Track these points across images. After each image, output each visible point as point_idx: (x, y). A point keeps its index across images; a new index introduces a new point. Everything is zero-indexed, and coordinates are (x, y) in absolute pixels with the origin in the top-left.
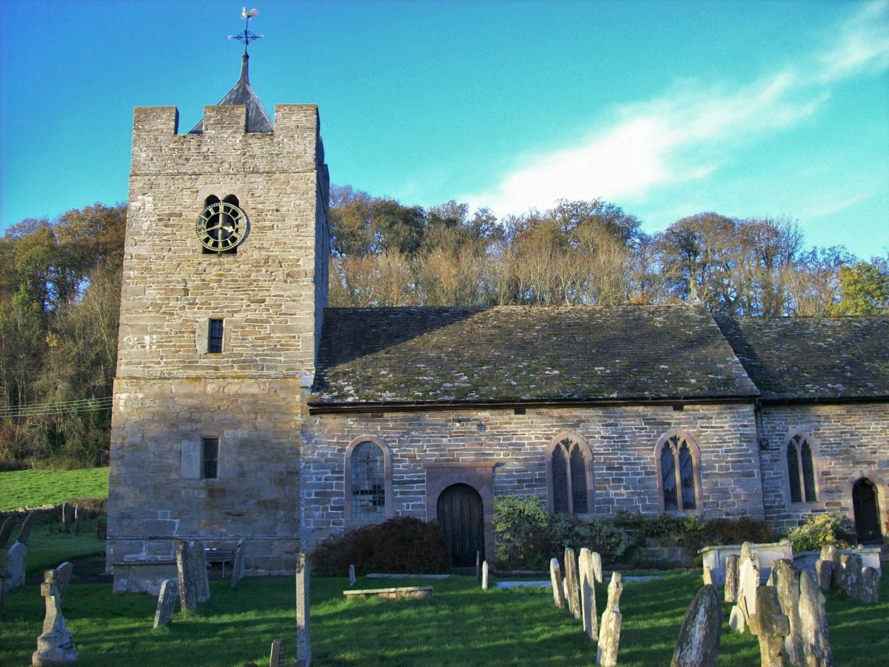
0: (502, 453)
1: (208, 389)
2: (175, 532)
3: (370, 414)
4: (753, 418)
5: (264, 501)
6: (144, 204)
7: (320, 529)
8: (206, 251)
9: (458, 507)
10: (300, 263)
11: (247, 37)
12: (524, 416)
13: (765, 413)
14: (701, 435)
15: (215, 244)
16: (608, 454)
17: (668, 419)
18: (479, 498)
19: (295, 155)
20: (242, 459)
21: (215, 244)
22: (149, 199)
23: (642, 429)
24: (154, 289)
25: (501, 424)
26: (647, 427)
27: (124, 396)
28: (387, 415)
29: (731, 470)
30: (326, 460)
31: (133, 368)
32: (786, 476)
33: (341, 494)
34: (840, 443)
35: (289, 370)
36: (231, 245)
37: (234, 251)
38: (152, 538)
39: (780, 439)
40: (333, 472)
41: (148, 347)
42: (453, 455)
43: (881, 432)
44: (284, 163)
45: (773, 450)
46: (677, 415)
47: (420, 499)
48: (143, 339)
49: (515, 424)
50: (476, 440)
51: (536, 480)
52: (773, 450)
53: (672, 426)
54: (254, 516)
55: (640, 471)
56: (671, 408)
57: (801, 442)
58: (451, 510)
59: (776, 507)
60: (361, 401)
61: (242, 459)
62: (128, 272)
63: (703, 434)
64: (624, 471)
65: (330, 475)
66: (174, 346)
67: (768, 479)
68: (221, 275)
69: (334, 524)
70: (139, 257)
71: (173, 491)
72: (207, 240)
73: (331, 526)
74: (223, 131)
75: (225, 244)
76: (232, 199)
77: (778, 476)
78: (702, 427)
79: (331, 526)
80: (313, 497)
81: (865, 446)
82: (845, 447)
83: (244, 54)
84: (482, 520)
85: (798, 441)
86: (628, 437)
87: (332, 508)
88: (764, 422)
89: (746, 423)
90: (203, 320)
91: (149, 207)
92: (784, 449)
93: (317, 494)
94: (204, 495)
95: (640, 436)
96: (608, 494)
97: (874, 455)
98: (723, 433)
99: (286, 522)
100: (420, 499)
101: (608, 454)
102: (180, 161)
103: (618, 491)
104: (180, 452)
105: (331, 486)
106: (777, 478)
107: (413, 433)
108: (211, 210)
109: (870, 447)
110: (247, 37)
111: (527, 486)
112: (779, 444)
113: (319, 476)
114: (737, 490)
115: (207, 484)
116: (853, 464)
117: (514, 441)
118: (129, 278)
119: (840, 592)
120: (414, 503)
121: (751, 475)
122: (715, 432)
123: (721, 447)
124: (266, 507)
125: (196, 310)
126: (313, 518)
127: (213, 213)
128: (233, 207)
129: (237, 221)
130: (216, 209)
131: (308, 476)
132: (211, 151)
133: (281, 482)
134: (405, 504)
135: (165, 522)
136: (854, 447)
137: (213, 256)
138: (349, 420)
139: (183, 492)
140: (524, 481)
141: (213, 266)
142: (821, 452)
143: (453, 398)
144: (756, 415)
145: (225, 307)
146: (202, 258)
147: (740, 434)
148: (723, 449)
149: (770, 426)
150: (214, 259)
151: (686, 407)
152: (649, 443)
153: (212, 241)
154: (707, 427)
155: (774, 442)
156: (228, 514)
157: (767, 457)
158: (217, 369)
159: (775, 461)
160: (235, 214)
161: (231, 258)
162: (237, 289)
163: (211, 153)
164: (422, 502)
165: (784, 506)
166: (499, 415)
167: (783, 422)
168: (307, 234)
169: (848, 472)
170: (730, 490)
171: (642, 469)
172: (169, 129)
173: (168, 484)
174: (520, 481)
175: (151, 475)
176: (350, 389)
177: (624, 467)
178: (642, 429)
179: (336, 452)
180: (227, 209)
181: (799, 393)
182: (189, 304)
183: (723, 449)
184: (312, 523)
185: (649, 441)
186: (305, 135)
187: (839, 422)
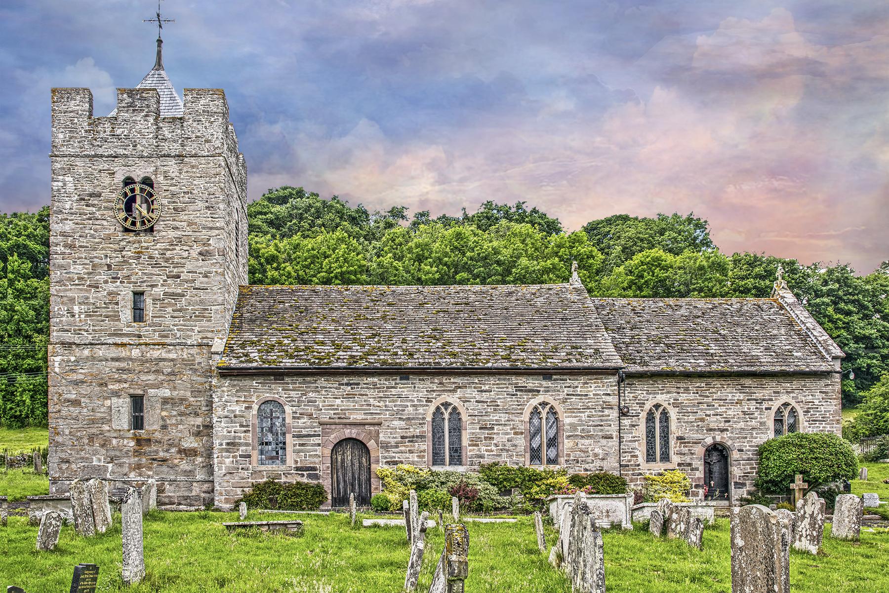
0: (388, 413)
1: (133, 354)
2: (108, 474)
3: (272, 378)
4: (616, 388)
5: (185, 450)
6: (65, 184)
7: (231, 473)
8: (126, 230)
9: (349, 458)
10: (211, 242)
13: (628, 384)
15: (134, 224)
16: (482, 416)
17: (538, 387)
18: (368, 451)
19: (203, 139)
20: (164, 413)
21: (134, 224)
22: (69, 179)
23: (513, 395)
24: (80, 265)
25: (388, 388)
27: (58, 359)
28: (287, 379)
30: (235, 416)
31: (64, 334)
32: (643, 439)
33: (247, 445)
35: (203, 338)
36: (148, 225)
37: (151, 230)
40: (242, 426)
41: (77, 316)
42: (345, 414)
43: (737, 403)
44: (190, 148)
45: (633, 416)
47: (316, 451)
48: (73, 308)
49: (400, 388)
50: (365, 401)
51: (417, 437)
52: (633, 416)
53: (541, 393)
54: (176, 461)
55: (509, 431)
56: (542, 377)
57: (661, 409)
58: (343, 461)
59: (631, 465)
60: (263, 366)
61: (164, 413)
62: (55, 248)
64: (495, 431)
65: (238, 428)
66: (101, 315)
67: (626, 441)
68: (139, 253)
69: (242, 469)
70: (63, 234)
71: (106, 440)
72: (126, 219)
73: (240, 471)
74: (135, 114)
75: (143, 223)
76: (147, 182)
79: (240, 471)
80: (224, 446)
84: (370, 469)
85: (657, 410)
86: (501, 402)
87: (241, 456)
88: (626, 392)
90: (126, 294)
91: (70, 187)
92: (643, 415)
93: (228, 444)
94: (132, 444)
96: (479, 450)
97: (727, 424)
99: (203, 467)
100: (316, 451)
101: (482, 416)
102: (96, 143)
103: (489, 448)
104: (110, 407)
105: (240, 438)
107: (310, 394)
108: (127, 191)
109: (725, 416)
111: (409, 441)
113: (229, 429)
114: (596, 450)
115: (135, 434)
116: (707, 431)
117: (399, 403)
118: (56, 253)
120: (311, 453)
122: (580, 399)
123: (584, 412)
124: (186, 454)
125: (118, 283)
126: (225, 464)
127: (130, 195)
128: (148, 189)
129: (152, 202)
130: (133, 190)
131: (220, 429)
132: (125, 133)
133: (198, 434)
134: (303, 454)
135: (99, 466)
136: (709, 416)
137: (132, 234)
138: (254, 382)
139: (114, 441)
140: (406, 437)
141: (131, 244)
142: (678, 419)
143: (345, 365)
144: (619, 385)
145: (144, 282)
147: (603, 402)
148: (586, 414)
149: (632, 395)
150: (131, 237)
151: (554, 377)
152: (519, 407)
153: (130, 219)
154: (573, 395)
156: (154, 459)
157: (626, 422)
158: (140, 336)
159: (634, 426)
160: (151, 195)
161: (149, 238)
162: (156, 265)
163: (125, 135)
164: (318, 453)
165: (639, 465)
167: (645, 392)
168: (217, 216)
169: (701, 438)
171: (511, 429)
172: (84, 111)
173: (100, 434)
174: (402, 437)
175: (86, 426)
176: (255, 355)
177: (496, 427)
178: (513, 395)
179: (243, 409)
180: (142, 190)
181: (661, 367)
182: (113, 278)
184: (224, 468)
185: (518, 405)
186: (212, 119)
187: (697, 393)
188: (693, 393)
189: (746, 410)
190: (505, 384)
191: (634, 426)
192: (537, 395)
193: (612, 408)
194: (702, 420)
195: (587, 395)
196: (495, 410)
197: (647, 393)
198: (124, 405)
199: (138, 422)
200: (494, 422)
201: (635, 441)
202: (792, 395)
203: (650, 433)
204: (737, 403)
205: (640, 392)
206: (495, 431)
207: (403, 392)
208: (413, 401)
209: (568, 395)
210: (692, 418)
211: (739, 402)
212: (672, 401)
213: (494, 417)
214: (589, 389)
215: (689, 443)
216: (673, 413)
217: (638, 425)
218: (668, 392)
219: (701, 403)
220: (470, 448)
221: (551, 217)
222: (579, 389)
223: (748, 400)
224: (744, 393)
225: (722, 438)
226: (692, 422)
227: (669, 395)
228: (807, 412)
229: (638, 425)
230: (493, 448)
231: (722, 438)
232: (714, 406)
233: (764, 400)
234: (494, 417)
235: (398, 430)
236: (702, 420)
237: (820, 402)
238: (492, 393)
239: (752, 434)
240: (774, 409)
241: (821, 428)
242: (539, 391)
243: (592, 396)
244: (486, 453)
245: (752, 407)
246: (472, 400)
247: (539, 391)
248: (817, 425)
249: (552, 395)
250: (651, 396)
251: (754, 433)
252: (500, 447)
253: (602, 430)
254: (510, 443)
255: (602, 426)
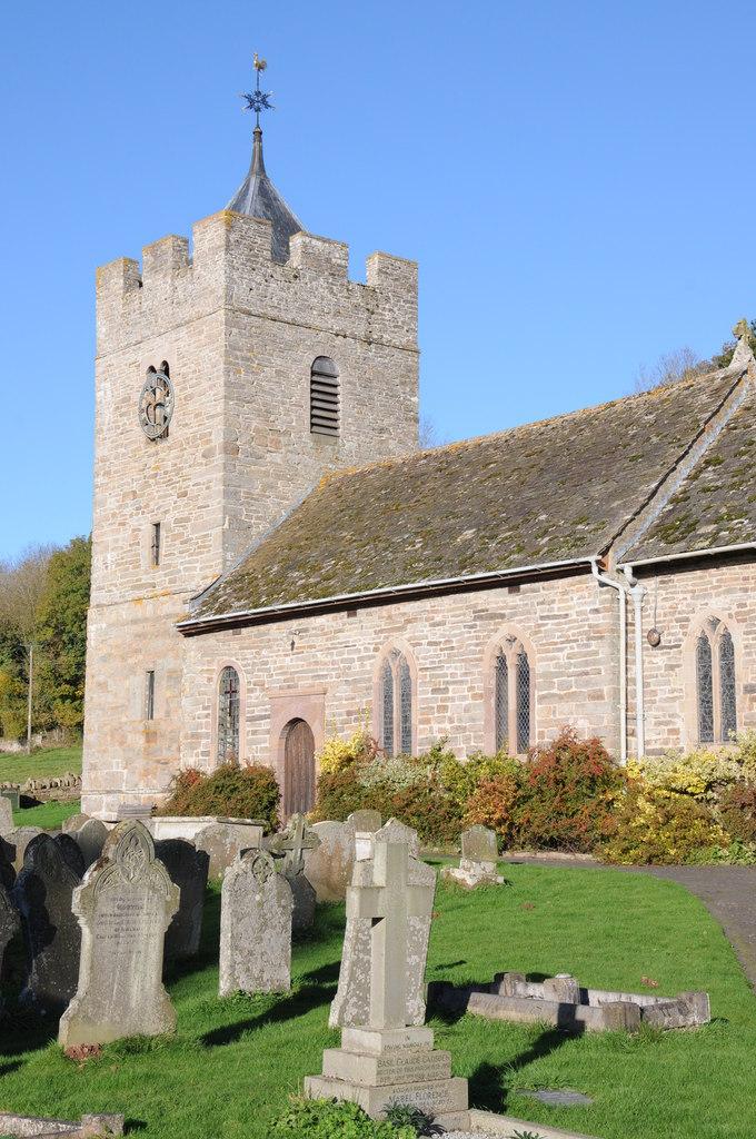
11: (258, 102)
14: (540, 632)
26: (478, 623)
29: (574, 689)
45: (671, 648)
52: (671, 648)
63: (543, 629)
64: (450, 694)
77: (676, 694)
78: (542, 618)
83: (253, 129)
88: (659, 599)
95: (469, 638)
98: (566, 627)
110: (258, 102)
112: (680, 636)
117: (345, 656)
119: (451, 888)
121: (600, 697)
122: (558, 624)
142: (746, 647)
146: (152, 448)
148: (566, 652)
152: (478, 649)
154: (548, 617)
155: (673, 634)
159: (672, 667)
167: (689, 596)
178: (471, 627)
183: (566, 652)
190: (461, 608)
191: (672, 667)
192: (500, 624)
193: (601, 638)
197: (692, 598)
200: (449, 679)
203: (705, 678)
205: (681, 596)
206: (450, 694)
207: (350, 636)
208: (360, 651)
209: (542, 618)
212: (735, 609)
213: (449, 669)
214: (571, 603)
217: (678, 666)
218: (729, 591)
220: (422, 726)
222: (555, 606)
227: (730, 597)
229: (678, 666)
234: (449, 669)
235: (344, 702)
238: (446, 627)
243: (574, 617)
246: (423, 641)
249: (521, 621)
250: (699, 602)
252: (456, 724)
254: (467, 715)
255: (587, 674)
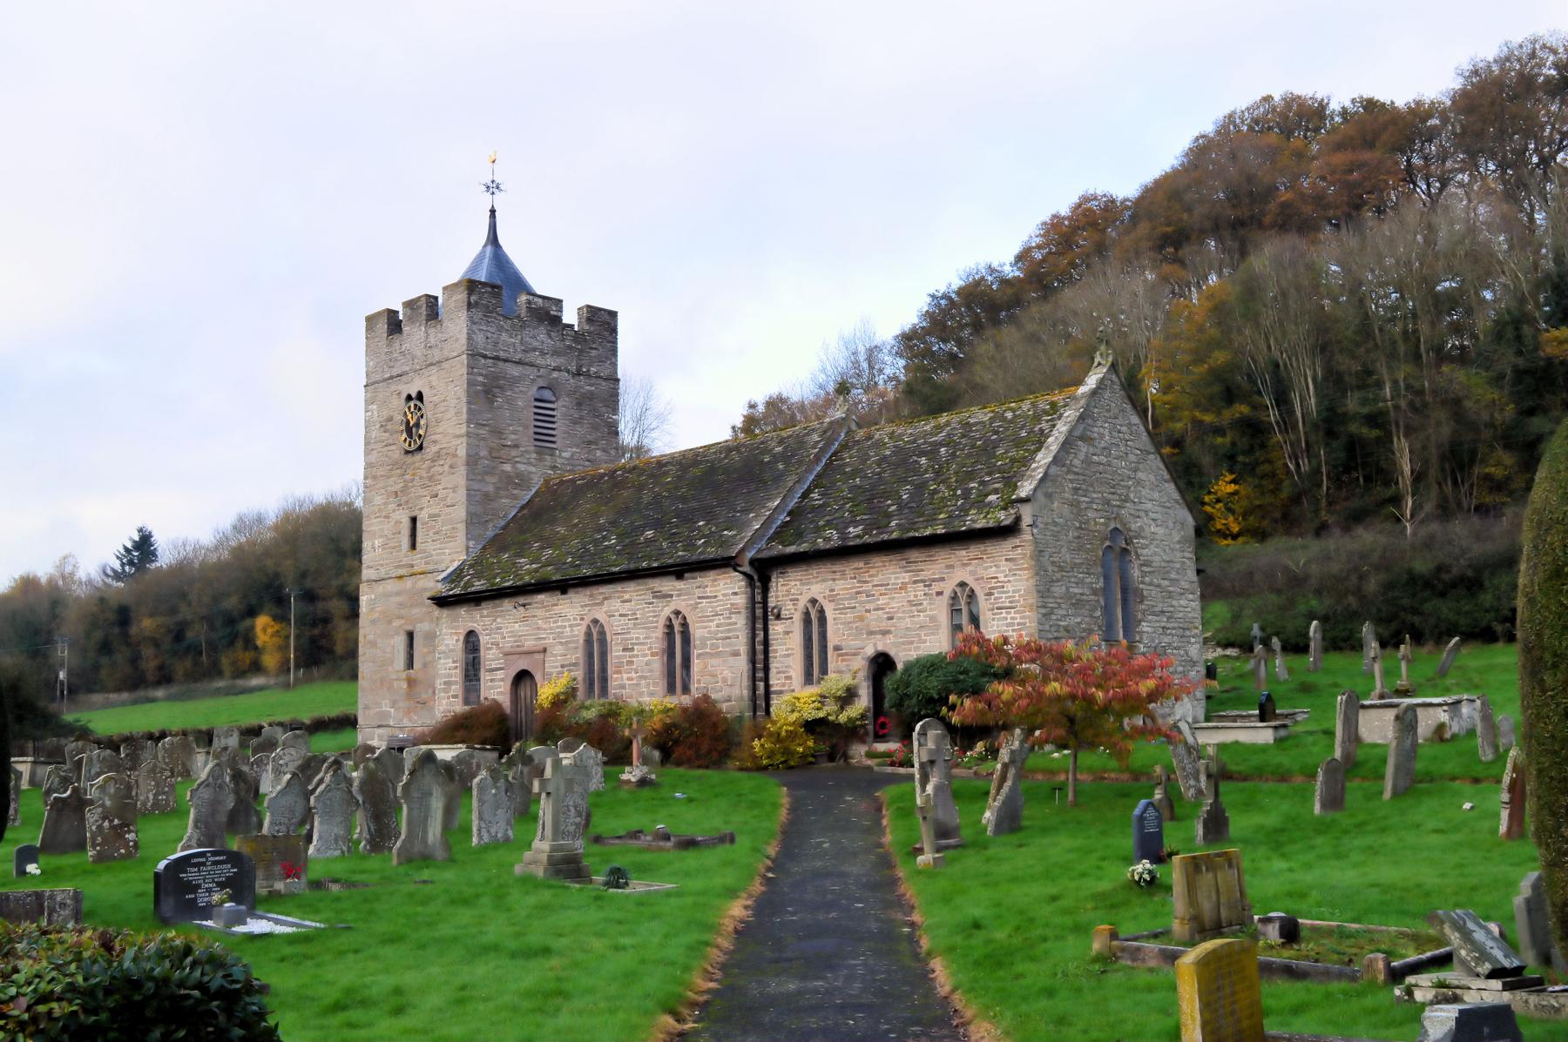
12: (1017, 541)
23: (650, 603)
34: (855, 607)
38: (379, 726)
39: (794, 605)
43: (901, 588)
46: (680, 585)
53: (674, 598)
64: (635, 652)
78: (699, 598)
81: (882, 609)
82: (859, 611)
89: (736, 590)
92: (798, 617)
94: (405, 685)
106: (788, 655)
116: (867, 634)
123: (712, 621)
149: (785, 588)
166: (551, 596)
167: (798, 583)
169: (860, 646)
170: (719, 672)
174: (562, 666)
187: (855, 578)
188: (851, 578)
189: (912, 598)
194: (861, 619)
195: (716, 597)
196: (634, 624)
197: (801, 584)
198: (400, 642)
199: (410, 664)
201: (788, 655)
202: (969, 568)
204: (901, 588)
210: (850, 616)
211: (903, 587)
213: (634, 634)
215: (847, 654)
216: (829, 615)
219: (858, 593)
221: (1258, 98)
222: (708, 589)
223: (915, 582)
224: (909, 571)
225: (885, 644)
226: (850, 623)
228: (990, 594)
230: (634, 675)
231: (885, 644)
232: (873, 595)
233: (934, 580)
236: (861, 619)
237: (1005, 577)
239: (919, 636)
240: (948, 593)
241: (1009, 621)
242: (671, 596)
244: (628, 682)
245: (918, 593)
247: (671, 596)
248: (1004, 615)
251: (923, 633)
253: (729, 645)
255: (729, 638)
